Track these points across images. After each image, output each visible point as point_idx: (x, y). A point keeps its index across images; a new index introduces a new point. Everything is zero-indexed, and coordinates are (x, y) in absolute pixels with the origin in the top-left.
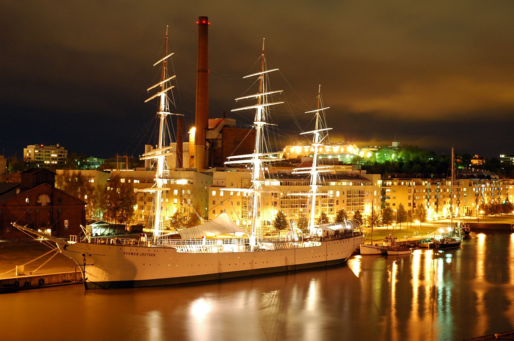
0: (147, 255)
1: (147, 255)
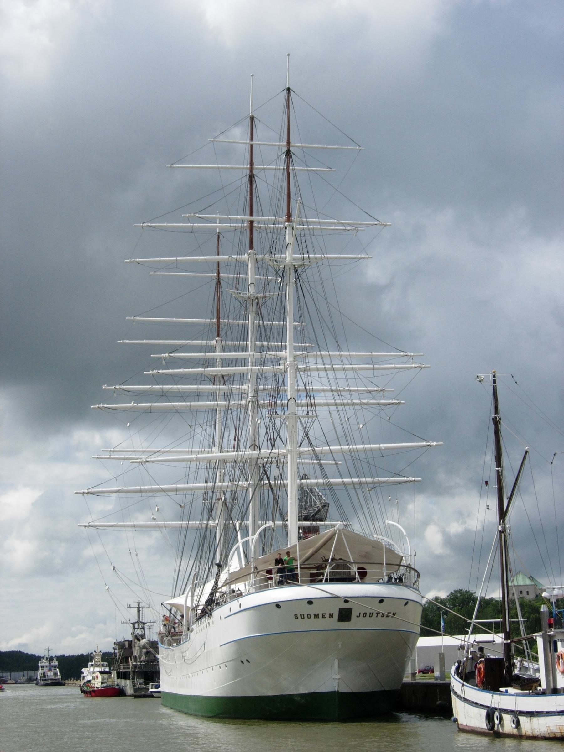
0: (375, 615)
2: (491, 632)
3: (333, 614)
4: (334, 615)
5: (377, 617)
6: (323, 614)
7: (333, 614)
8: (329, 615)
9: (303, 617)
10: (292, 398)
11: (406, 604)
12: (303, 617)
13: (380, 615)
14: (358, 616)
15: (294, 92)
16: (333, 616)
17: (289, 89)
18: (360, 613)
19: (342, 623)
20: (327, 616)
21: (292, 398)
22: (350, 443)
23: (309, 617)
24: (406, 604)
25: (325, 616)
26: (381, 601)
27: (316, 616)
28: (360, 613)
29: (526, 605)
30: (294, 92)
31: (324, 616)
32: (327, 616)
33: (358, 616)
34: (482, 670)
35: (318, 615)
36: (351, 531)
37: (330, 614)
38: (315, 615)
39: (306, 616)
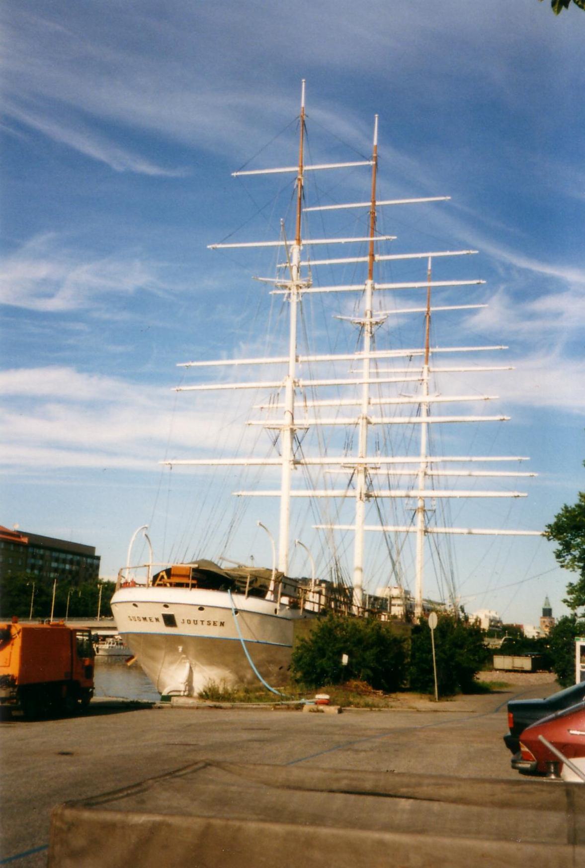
0: (199, 623)
18: (183, 620)
28: (183, 620)
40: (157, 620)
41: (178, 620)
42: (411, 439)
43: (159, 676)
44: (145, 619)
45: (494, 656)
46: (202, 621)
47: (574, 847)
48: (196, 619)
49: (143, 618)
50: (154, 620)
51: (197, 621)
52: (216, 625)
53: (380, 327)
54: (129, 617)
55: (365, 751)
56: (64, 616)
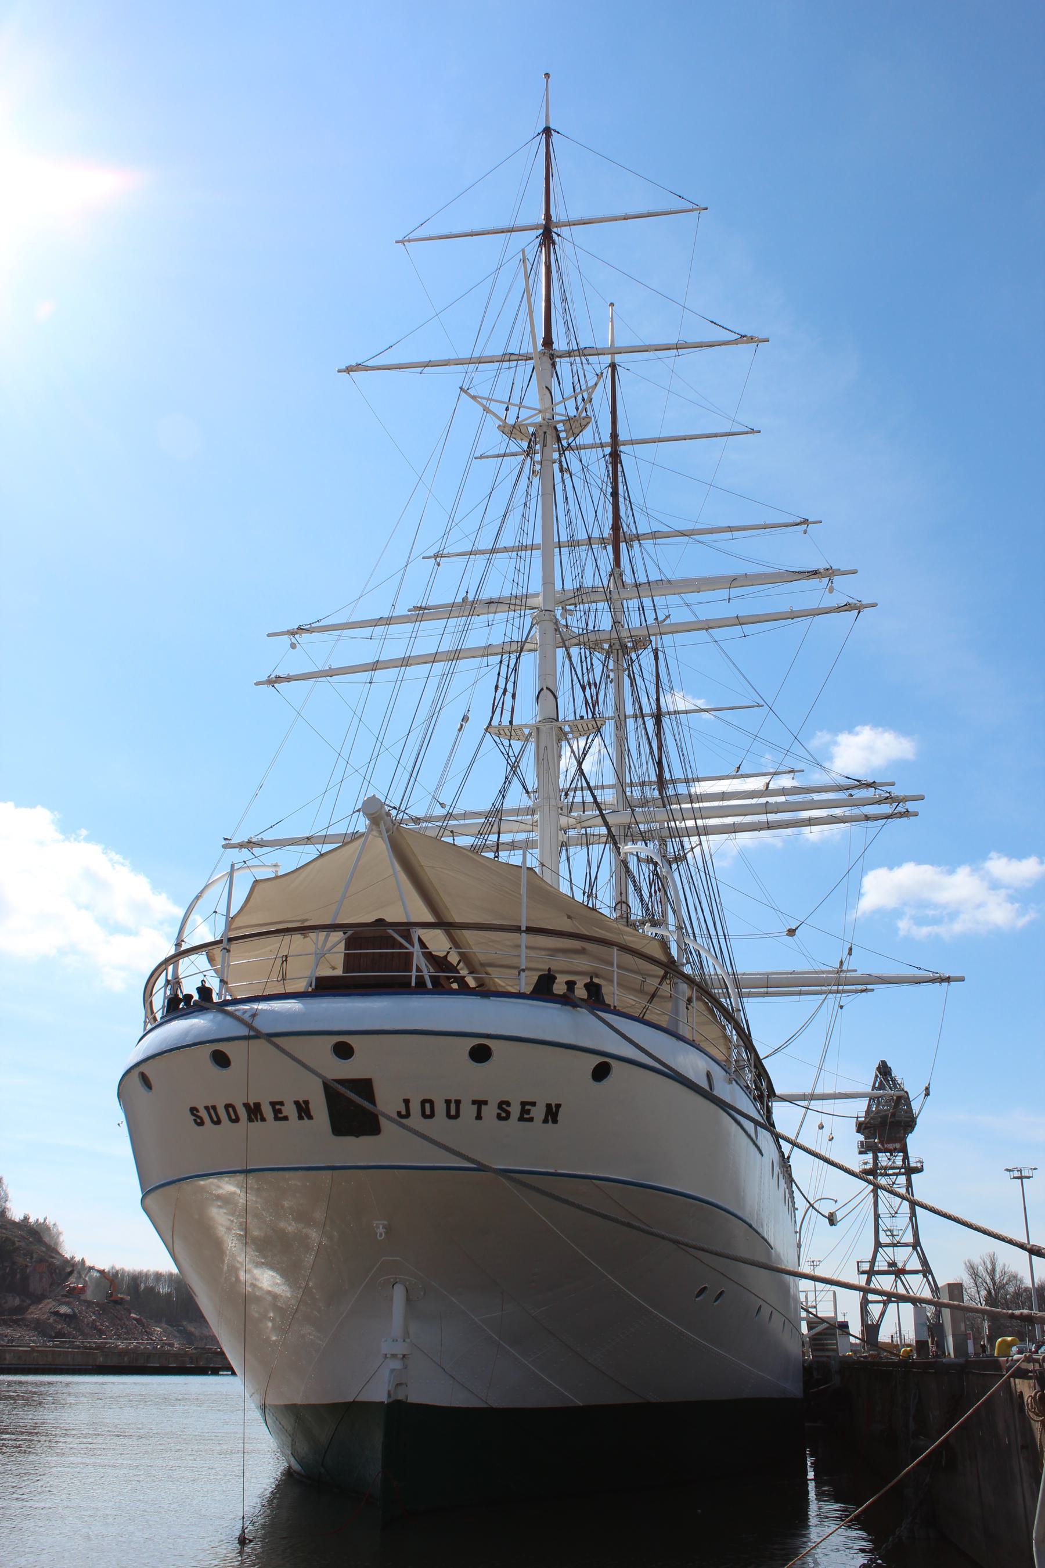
0: (468, 1111)
1: (468, 1111)
2: (815, 1337)
3: (558, 1106)
4: (311, 1106)
5: (479, 1117)
6: (523, 1104)
7: (558, 1106)
8: (544, 1110)
9: (453, 1112)
10: (545, 688)
11: (601, 1072)
12: (453, 1112)
13: (490, 1111)
14: (404, 1112)
15: (558, 133)
16: (312, 1113)
17: (547, 131)
18: (407, 1102)
19: (349, 1141)
20: (538, 1112)
21: (545, 688)
22: (700, 800)
23: (428, 1112)
24: (601, 1072)
25: (284, 1114)
26: (480, 1054)
27: (254, 1112)
28: (407, 1102)
29: (300, 1287)
30: (558, 133)
31: (528, 1112)
32: (538, 1112)
33: (404, 1112)
34: (843, 1505)
35: (258, 1105)
36: (583, 904)
37: (549, 1106)
38: (246, 1105)
39: (440, 1108)
40: (304, 1110)
41: (387, 1101)
42: (584, 803)
43: (294, 1471)
44: (254, 1112)
45: (454, 1114)
46: (480, 1104)
47: (283, 1284)
48: (453, 1098)
49: (246, 1105)
50: (290, 1110)
51: (458, 1102)
52: (531, 1120)
53: (604, 457)
54: (193, 1110)
55: (114, 1315)
56: (421, 949)
